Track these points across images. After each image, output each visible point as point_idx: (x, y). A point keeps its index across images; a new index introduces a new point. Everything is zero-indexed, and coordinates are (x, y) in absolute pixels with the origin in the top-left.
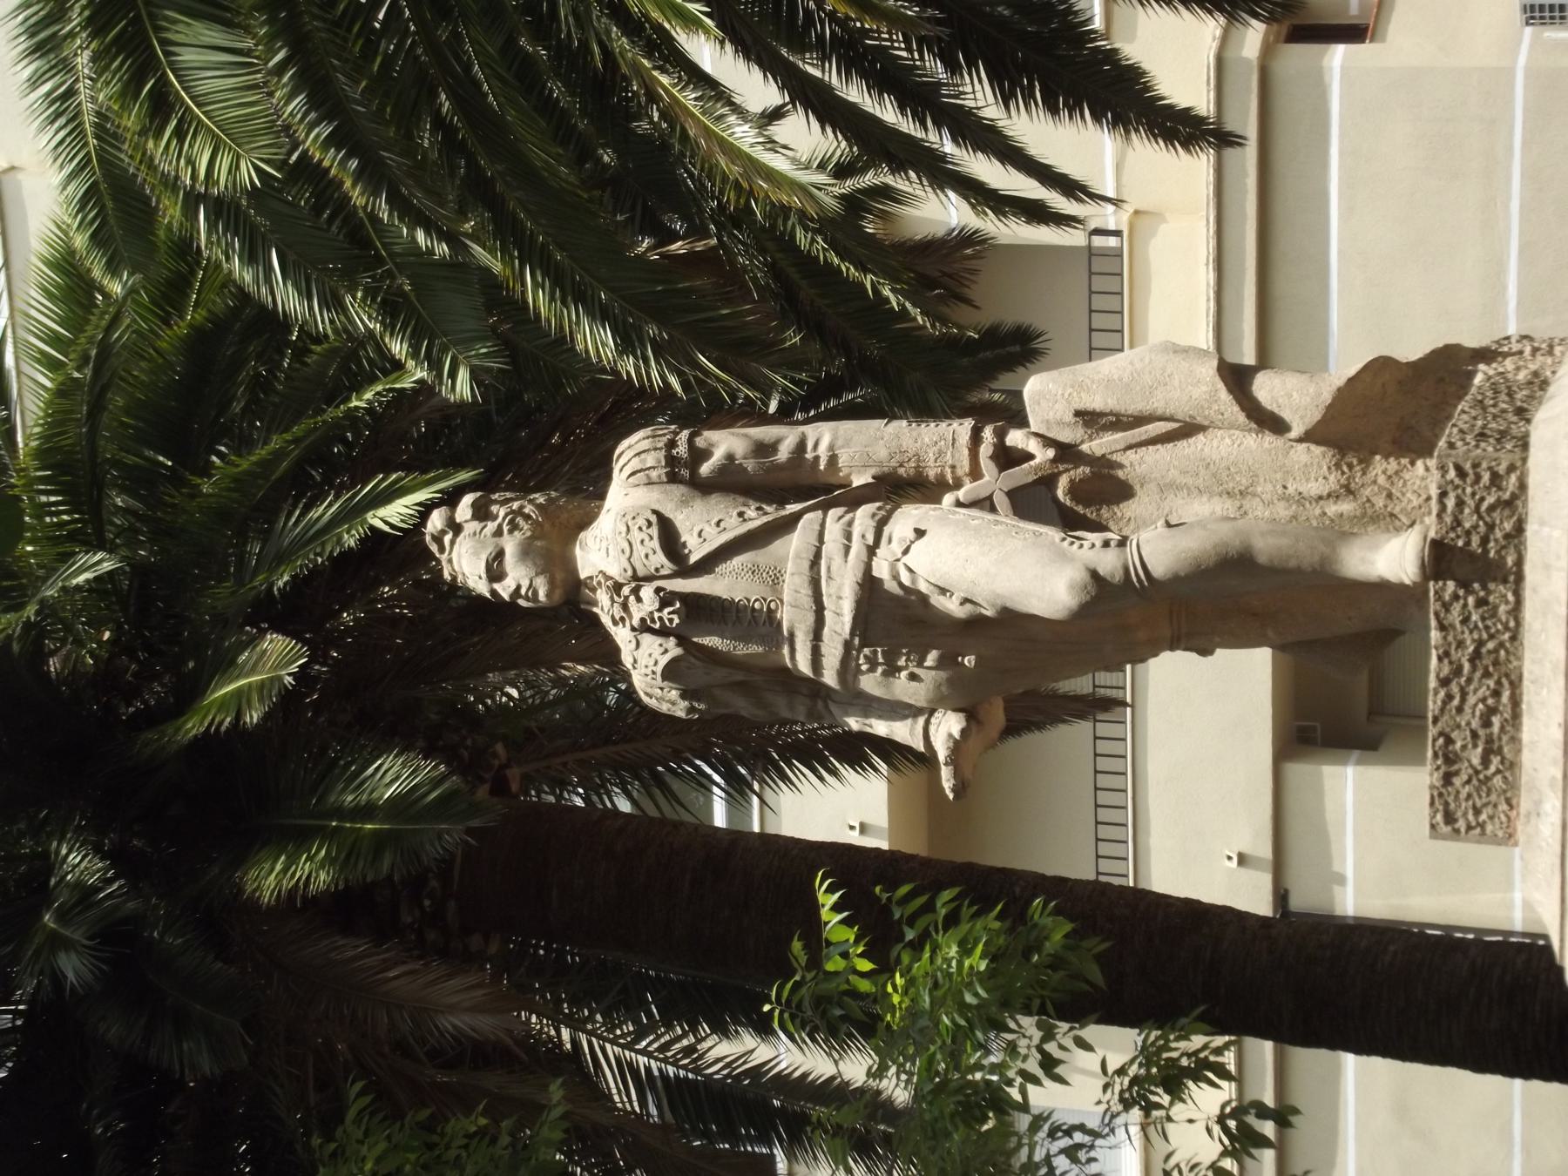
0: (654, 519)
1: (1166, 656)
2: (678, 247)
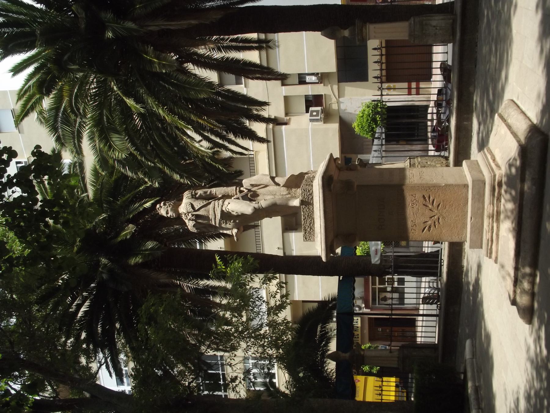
1: (265, 219)
2: (188, 162)
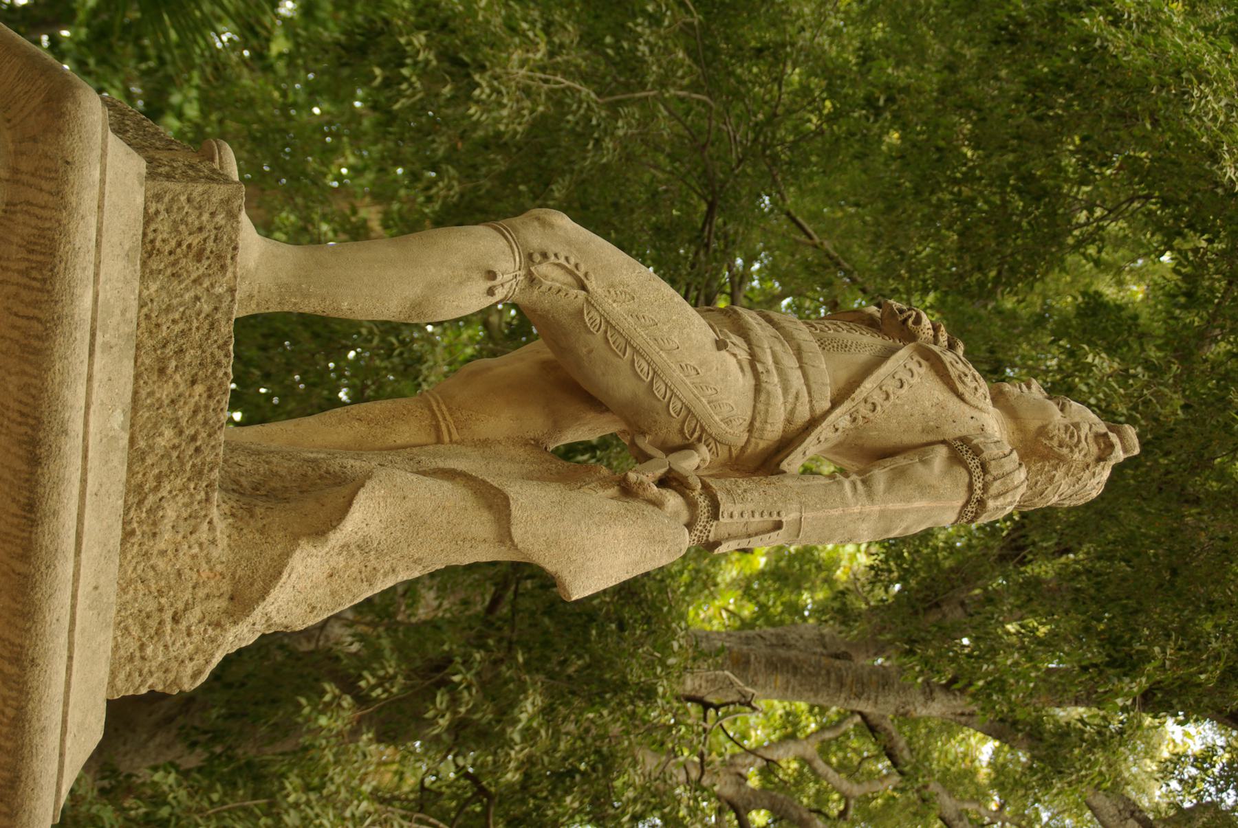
0: (960, 387)
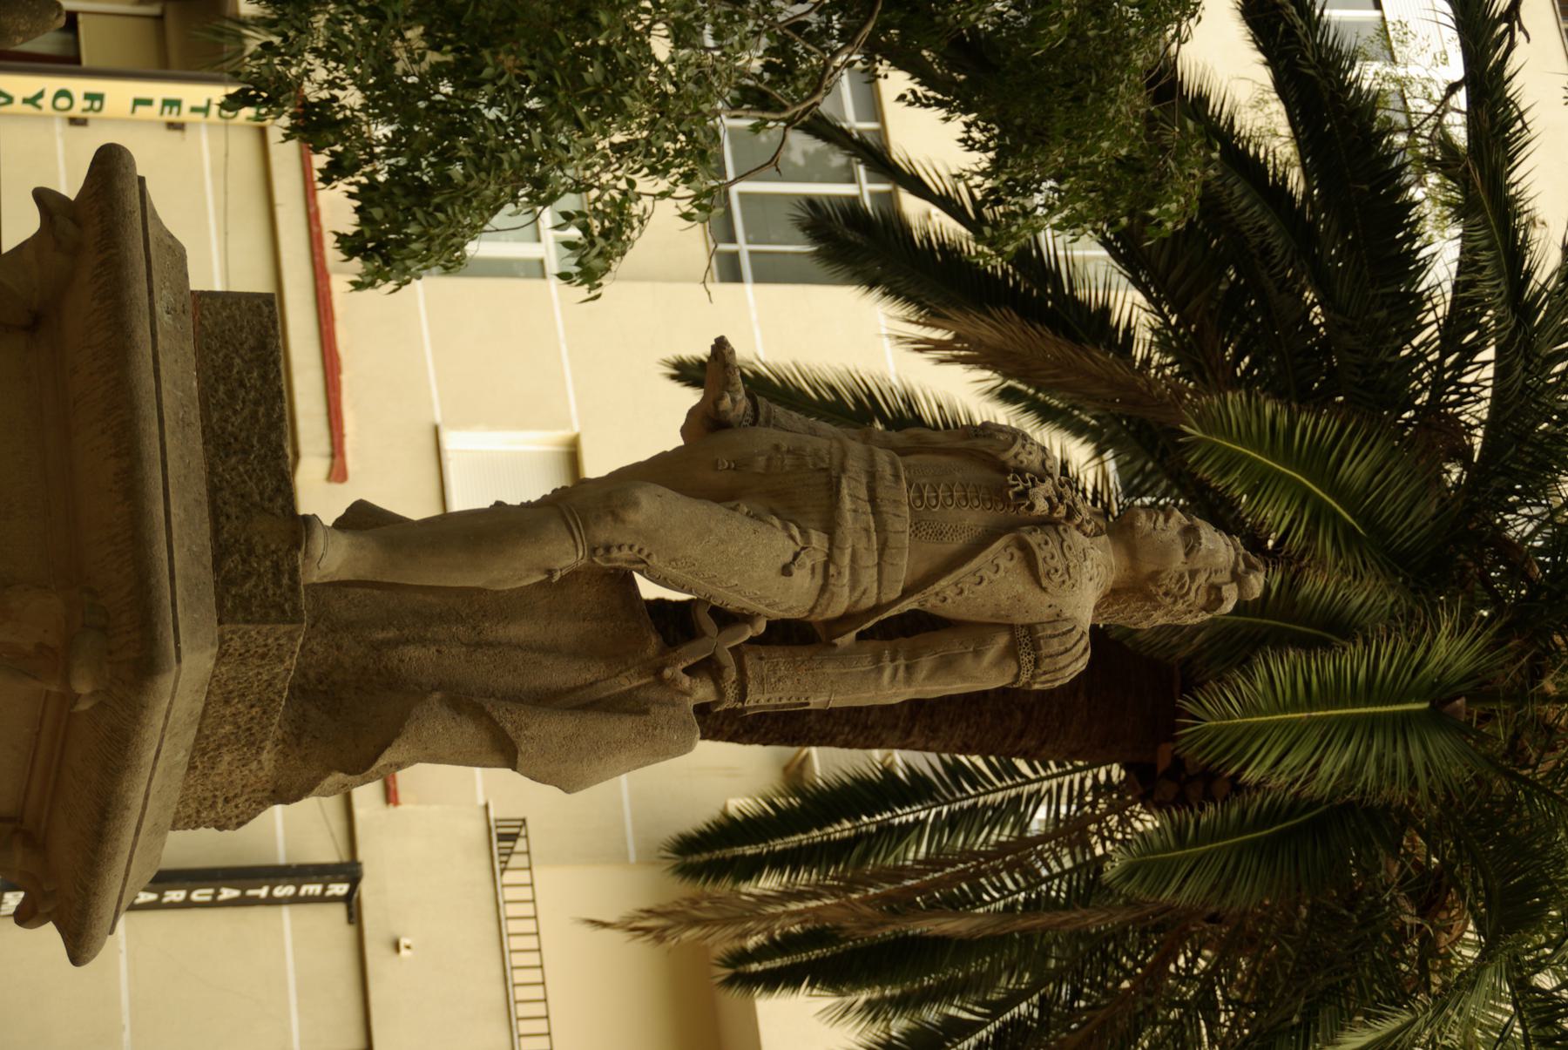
0: (1045, 582)
